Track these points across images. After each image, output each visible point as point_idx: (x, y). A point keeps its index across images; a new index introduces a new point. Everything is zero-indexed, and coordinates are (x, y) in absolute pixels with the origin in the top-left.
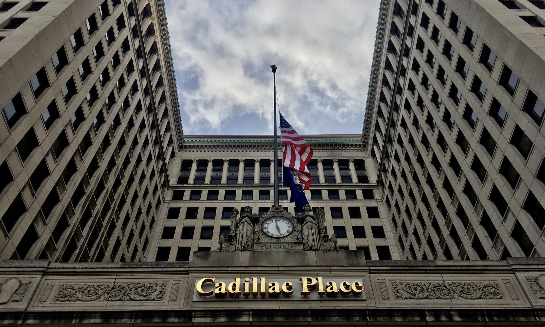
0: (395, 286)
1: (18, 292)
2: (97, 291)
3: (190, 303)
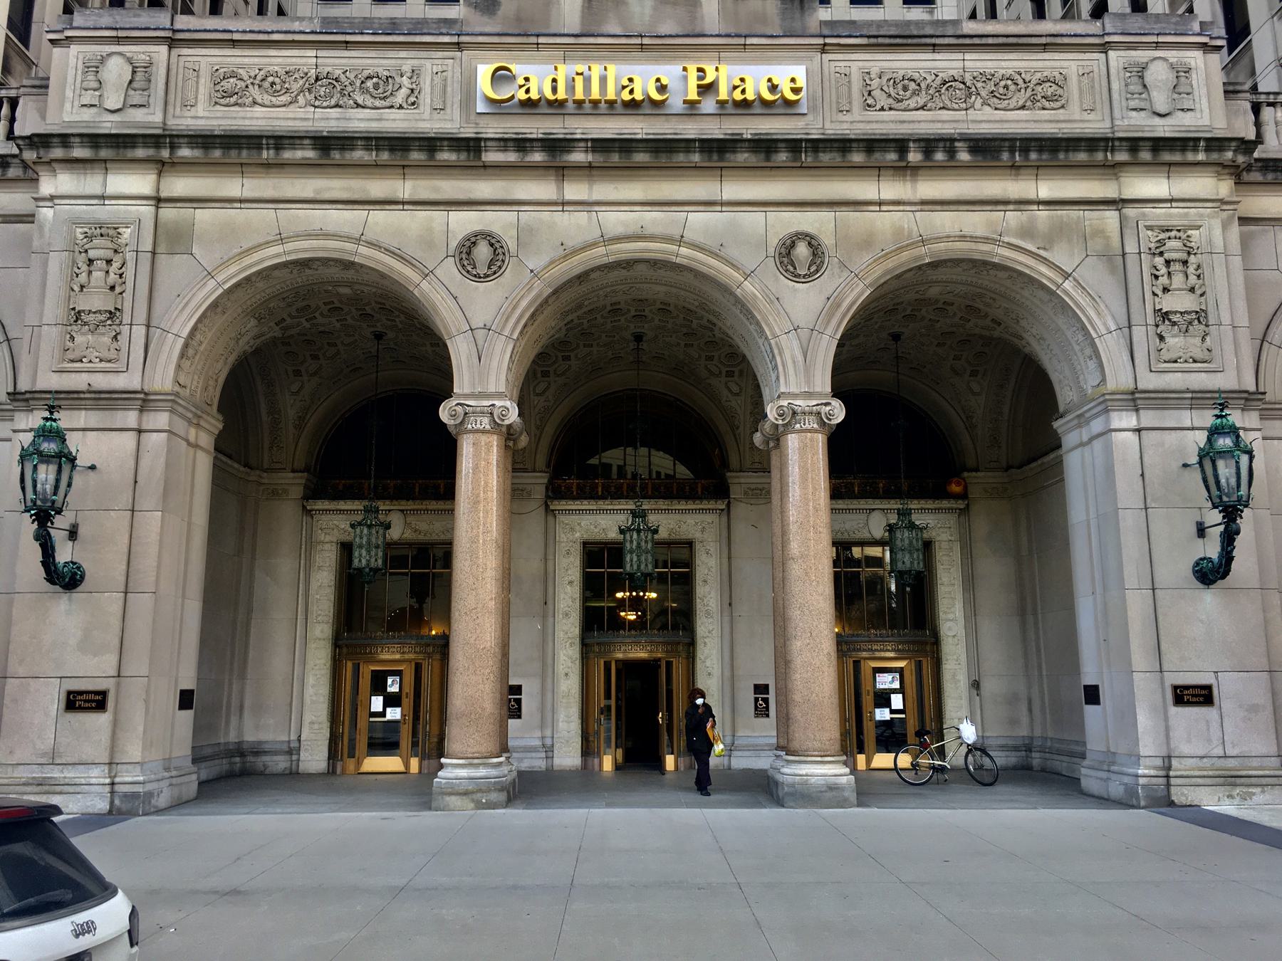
0: (868, 82)
1: (135, 85)
2: (286, 86)
3: (473, 117)
